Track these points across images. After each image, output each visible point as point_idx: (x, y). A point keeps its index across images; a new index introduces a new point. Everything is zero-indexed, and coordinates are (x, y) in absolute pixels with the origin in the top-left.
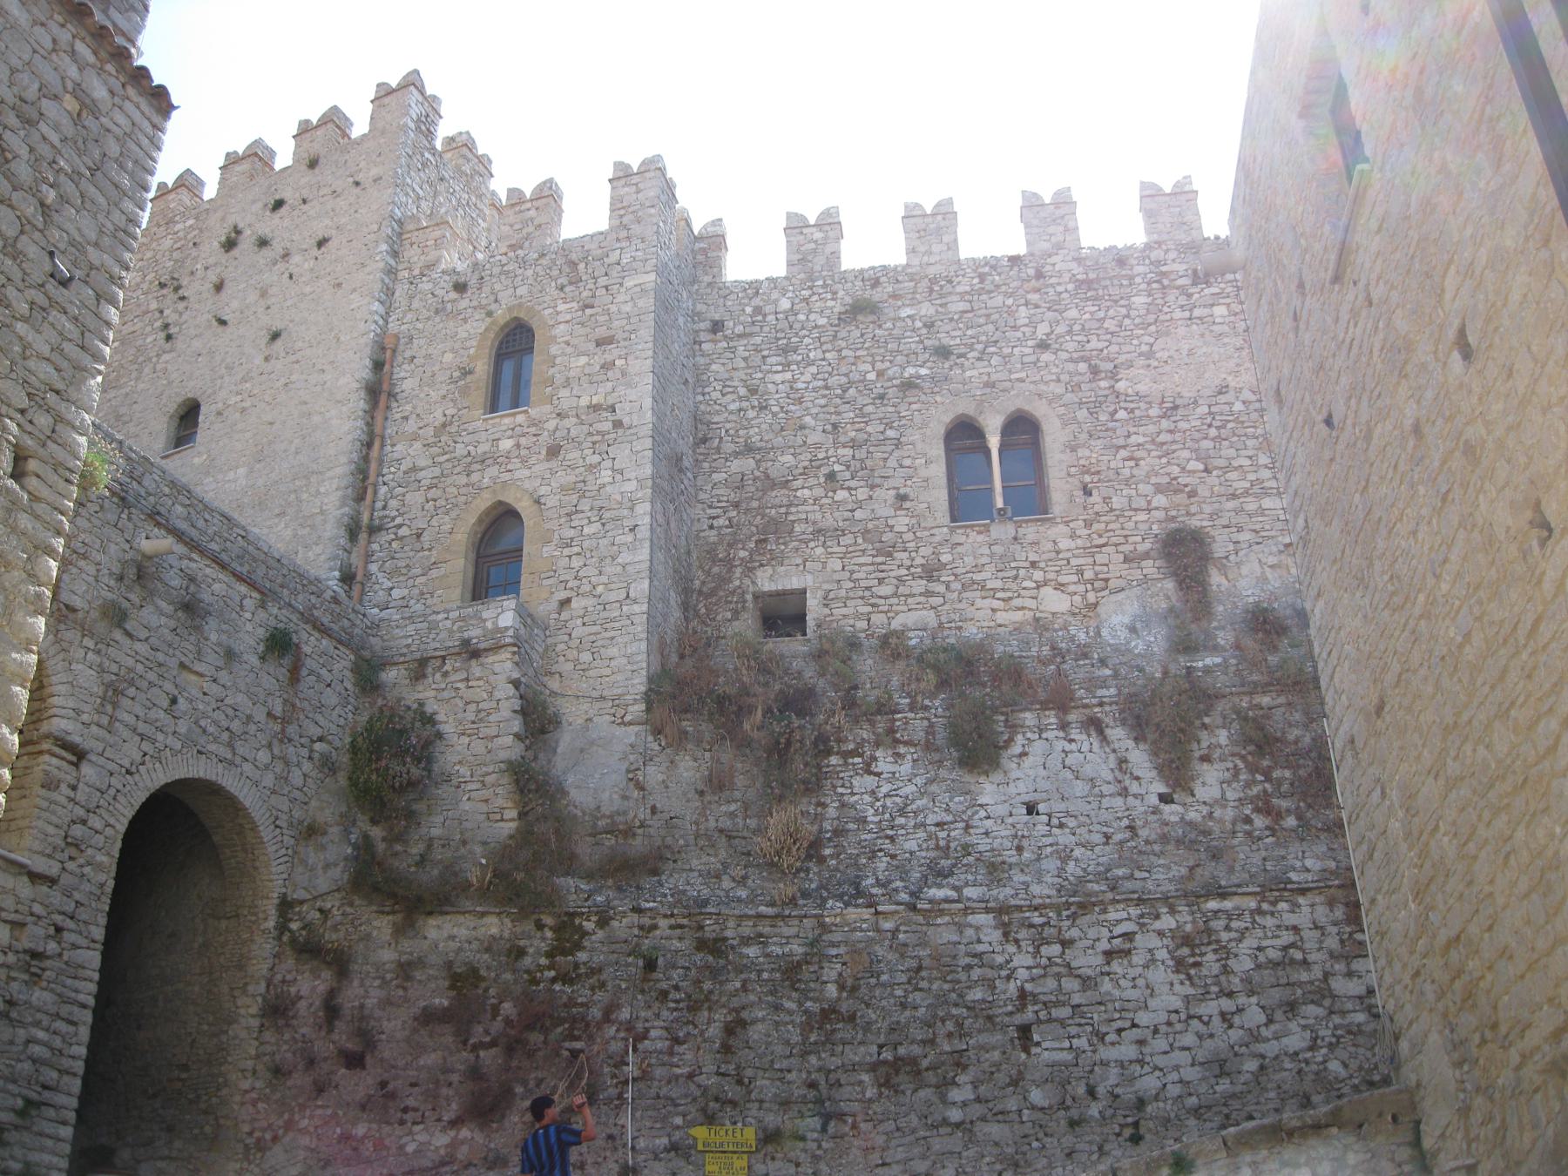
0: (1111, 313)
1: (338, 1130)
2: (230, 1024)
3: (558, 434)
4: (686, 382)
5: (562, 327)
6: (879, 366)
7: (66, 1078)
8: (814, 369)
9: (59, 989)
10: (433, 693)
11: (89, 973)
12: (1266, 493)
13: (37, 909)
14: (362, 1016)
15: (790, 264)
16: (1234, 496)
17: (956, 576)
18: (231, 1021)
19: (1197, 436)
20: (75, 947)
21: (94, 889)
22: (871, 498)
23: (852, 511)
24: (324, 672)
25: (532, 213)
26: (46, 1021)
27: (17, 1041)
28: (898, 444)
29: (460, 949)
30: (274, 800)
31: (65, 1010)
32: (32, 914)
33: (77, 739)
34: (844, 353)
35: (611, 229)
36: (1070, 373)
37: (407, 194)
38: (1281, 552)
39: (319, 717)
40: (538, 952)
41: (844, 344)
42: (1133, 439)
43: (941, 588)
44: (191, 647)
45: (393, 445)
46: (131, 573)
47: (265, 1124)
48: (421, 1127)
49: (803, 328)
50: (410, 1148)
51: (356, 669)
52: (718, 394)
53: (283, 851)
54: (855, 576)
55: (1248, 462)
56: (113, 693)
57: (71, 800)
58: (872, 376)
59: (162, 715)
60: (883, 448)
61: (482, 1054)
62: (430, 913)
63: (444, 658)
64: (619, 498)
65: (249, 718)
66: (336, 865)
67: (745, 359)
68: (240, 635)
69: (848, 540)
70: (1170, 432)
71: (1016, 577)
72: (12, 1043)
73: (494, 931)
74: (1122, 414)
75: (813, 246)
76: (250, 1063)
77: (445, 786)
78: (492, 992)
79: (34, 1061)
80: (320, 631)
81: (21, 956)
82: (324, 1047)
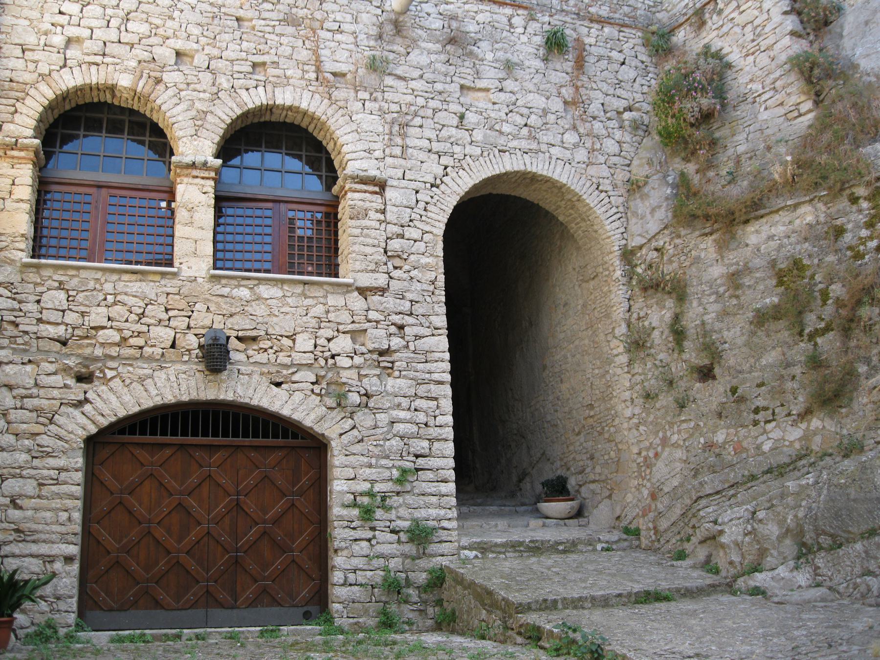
1: (702, 440)
7: (436, 445)
9: (412, 374)
10: (715, 33)
11: (440, 355)
13: (373, 315)
14: (704, 330)
18: (609, 361)
20: (418, 337)
21: (425, 287)
24: (614, 54)
27: (380, 424)
29: (781, 246)
30: (592, 170)
31: (422, 390)
33: (373, 173)
39: (619, 92)
40: (858, 227)
44: (468, 71)
46: (389, 28)
47: (647, 444)
48: (773, 424)
50: (766, 447)
53: (614, 210)
56: (400, 125)
59: (453, 131)
61: (819, 340)
62: (747, 222)
65: (545, 112)
66: (660, 207)
68: (517, 47)
72: (376, 427)
73: (809, 218)
76: (628, 393)
77: (743, 107)
78: (818, 278)
80: (598, 22)
81: (368, 356)
82: (678, 368)
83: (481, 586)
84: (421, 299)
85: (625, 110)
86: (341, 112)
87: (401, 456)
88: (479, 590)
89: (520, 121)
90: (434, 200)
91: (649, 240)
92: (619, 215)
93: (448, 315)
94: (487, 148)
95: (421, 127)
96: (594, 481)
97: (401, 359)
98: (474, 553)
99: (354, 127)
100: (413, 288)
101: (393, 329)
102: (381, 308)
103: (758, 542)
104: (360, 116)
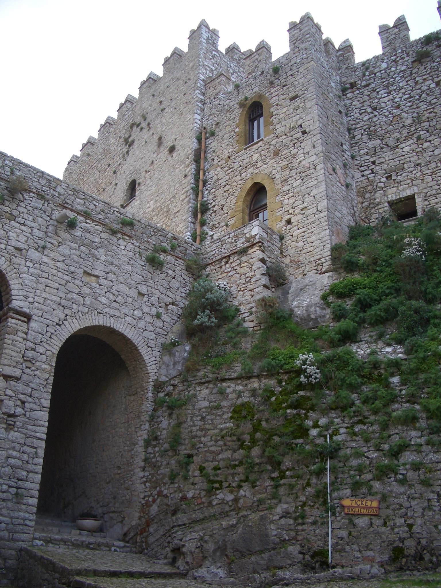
1: (181, 495)
2: (135, 445)
3: (277, 145)
4: (340, 112)
8: (403, 91)
9: (24, 431)
13: (9, 392)
15: (384, 48)
21: (42, 382)
23: (433, 151)
25: (257, 57)
26: (18, 447)
30: (145, 334)
32: (6, 395)
33: (26, 310)
34: (417, 79)
35: (291, 50)
37: (206, 69)
39: (169, 293)
41: (416, 75)
49: (395, 74)
51: (188, 268)
52: (358, 115)
53: (154, 359)
57: (24, 339)
58: (433, 85)
59: (75, 296)
63: (229, 256)
67: (368, 96)
69: (433, 165)
75: (394, 36)
79: (12, 467)
83: (47, 559)
84: (38, 388)
85: (170, 304)
86: (15, 270)
87: (10, 478)
88: (46, 561)
89: (112, 297)
90: (56, 333)
91: (170, 379)
92: (156, 362)
93: (51, 400)
94: (92, 308)
95: (57, 289)
96: (114, 512)
97: (20, 421)
98: (42, 542)
99: (21, 281)
100: (34, 381)
101: (19, 403)
102: (14, 389)
103: (202, 553)
104: (25, 275)
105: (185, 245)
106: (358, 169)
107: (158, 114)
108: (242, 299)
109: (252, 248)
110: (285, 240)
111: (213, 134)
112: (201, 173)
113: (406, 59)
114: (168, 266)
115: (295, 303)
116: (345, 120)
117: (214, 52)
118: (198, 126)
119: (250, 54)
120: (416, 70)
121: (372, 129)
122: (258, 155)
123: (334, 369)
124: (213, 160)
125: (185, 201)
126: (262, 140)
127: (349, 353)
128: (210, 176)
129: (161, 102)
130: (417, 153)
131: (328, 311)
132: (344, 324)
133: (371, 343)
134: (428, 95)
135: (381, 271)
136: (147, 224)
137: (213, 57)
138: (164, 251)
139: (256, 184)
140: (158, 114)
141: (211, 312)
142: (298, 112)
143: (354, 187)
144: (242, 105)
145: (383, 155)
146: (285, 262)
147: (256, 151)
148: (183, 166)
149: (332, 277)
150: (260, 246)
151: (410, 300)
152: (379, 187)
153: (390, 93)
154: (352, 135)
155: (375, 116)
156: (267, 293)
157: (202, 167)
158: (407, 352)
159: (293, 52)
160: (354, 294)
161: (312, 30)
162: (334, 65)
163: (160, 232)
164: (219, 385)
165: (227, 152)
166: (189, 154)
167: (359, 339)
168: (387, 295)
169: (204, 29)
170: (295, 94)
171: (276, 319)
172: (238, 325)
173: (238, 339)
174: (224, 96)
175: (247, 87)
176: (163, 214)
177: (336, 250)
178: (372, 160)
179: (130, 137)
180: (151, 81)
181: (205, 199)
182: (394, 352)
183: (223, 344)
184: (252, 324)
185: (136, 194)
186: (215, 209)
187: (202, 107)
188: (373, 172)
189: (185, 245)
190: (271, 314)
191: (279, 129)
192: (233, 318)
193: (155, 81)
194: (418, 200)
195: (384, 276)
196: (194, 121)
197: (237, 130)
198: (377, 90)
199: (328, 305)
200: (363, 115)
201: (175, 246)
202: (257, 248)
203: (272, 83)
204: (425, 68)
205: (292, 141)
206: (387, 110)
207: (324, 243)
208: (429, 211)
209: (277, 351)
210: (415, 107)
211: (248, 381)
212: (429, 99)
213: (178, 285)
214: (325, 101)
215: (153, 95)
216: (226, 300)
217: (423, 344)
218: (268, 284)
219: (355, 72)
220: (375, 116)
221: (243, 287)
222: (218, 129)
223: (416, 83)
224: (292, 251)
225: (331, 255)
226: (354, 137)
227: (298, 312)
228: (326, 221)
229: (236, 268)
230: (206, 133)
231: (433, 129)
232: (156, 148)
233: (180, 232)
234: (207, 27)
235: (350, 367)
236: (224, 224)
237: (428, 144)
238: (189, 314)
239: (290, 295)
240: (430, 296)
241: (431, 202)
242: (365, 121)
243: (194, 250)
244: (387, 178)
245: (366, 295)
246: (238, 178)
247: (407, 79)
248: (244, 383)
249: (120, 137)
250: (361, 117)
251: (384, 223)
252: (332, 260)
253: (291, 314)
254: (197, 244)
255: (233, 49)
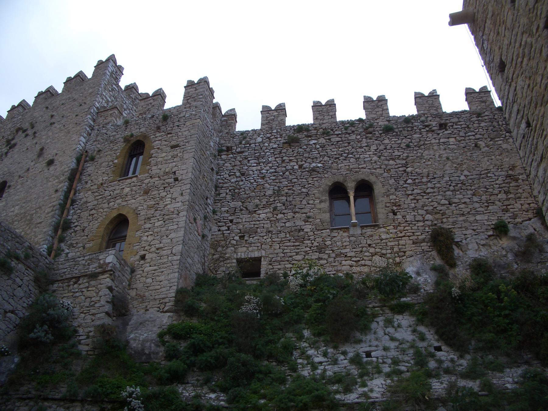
0: (404, 141)
3: (149, 185)
4: (212, 169)
5: (157, 142)
6: (300, 163)
8: (270, 165)
12: (478, 213)
15: (262, 124)
16: (463, 215)
17: (333, 251)
19: (444, 189)
22: (294, 217)
25: (152, 101)
28: (307, 194)
36: (385, 165)
38: (487, 239)
39: (11, 301)
41: (284, 155)
42: (415, 191)
43: (326, 256)
45: (79, 194)
51: (37, 280)
54: (285, 251)
55: (468, 200)
58: (296, 167)
60: (300, 196)
63: (79, 277)
64: (172, 210)
67: (240, 161)
69: (283, 235)
70: (432, 188)
71: (361, 252)
74: (409, 181)
75: (273, 117)
85: (10, 311)
105: (39, 257)
106: (216, 223)
107: (47, 127)
108: (82, 321)
109: (103, 275)
110: (135, 273)
111: (93, 159)
112: (72, 192)
113: (279, 139)
114: (17, 274)
115: (132, 336)
116: (215, 177)
117: (114, 86)
118: (81, 148)
119: (146, 97)
120: (285, 151)
121: (236, 191)
122: (129, 189)
123: (157, 406)
124: (86, 182)
125: (50, 215)
126: (137, 176)
127: (175, 393)
128: (80, 197)
129: (52, 116)
130: (271, 221)
131: (162, 349)
132: (175, 364)
133: (197, 386)
134: (290, 174)
135: (218, 321)
136: (7, 228)
137: (113, 90)
138: (17, 258)
139: (120, 215)
140: (47, 127)
141: (49, 327)
142: (175, 159)
143: (209, 239)
144: (126, 140)
145: (241, 216)
146: (131, 294)
147: (129, 185)
148: (56, 181)
149: (172, 317)
150: (111, 275)
151: (239, 352)
152: (231, 244)
153: (259, 164)
154: (217, 192)
155: (242, 181)
156: (108, 321)
157: (74, 187)
158: (228, 401)
159: (184, 106)
160: (189, 337)
161: (206, 92)
162: (217, 127)
163: (18, 239)
164: (40, 404)
165: (101, 179)
166: (66, 172)
167: (186, 382)
168: (220, 344)
169: (111, 63)
170: (177, 143)
171: (111, 347)
172: (74, 346)
173: (70, 360)
174: (113, 127)
175: (135, 125)
176: (25, 221)
177: (181, 293)
178: (230, 218)
179: (13, 139)
180: (50, 93)
181: (70, 217)
182: (217, 398)
183: (54, 362)
184: (86, 348)
185: (4, 196)
186: (76, 229)
187: (90, 131)
188: (229, 229)
189: (39, 257)
190: (107, 341)
191: (155, 170)
192: (70, 338)
193: (53, 95)
194: (264, 263)
195: (220, 326)
196: (80, 142)
197: (116, 161)
198: (249, 159)
199: (164, 343)
200: (232, 177)
201: (29, 255)
202: (108, 275)
203: (158, 128)
204: (293, 151)
205: (163, 184)
206: (253, 177)
207: (171, 285)
208: (271, 275)
209: (106, 379)
210: (278, 181)
211: (71, 404)
212: (291, 177)
213: (22, 294)
214: (201, 156)
215: (47, 108)
216: (67, 319)
217: (245, 396)
218: (111, 312)
219: (233, 138)
220: (242, 181)
221: (86, 309)
222: (98, 156)
223: (283, 161)
224: (140, 286)
225: (175, 297)
226: (219, 194)
227: (134, 344)
228: (177, 265)
229: (84, 290)
230: (86, 156)
231: (289, 204)
232: (35, 157)
233: (37, 243)
234: (115, 62)
235: (173, 407)
236: (81, 245)
237: (282, 215)
238: (26, 326)
239: (129, 327)
240: (259, 352)
241: (275, 267)
242: (232, 183)
243: (47, 263)
244: (240, 237)
245: (201, 340)
246: (106, 205)
247: (276, 156)
248: (67, 405)
249: (3, 137)
250: (229, 178)
251: (230, 278)
252: (175, 301)
253: (126, 346)
254: (51, 259)
255: (132, 88)
